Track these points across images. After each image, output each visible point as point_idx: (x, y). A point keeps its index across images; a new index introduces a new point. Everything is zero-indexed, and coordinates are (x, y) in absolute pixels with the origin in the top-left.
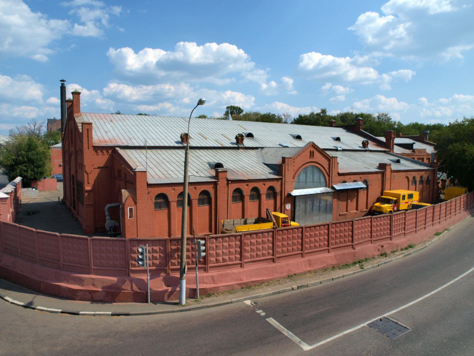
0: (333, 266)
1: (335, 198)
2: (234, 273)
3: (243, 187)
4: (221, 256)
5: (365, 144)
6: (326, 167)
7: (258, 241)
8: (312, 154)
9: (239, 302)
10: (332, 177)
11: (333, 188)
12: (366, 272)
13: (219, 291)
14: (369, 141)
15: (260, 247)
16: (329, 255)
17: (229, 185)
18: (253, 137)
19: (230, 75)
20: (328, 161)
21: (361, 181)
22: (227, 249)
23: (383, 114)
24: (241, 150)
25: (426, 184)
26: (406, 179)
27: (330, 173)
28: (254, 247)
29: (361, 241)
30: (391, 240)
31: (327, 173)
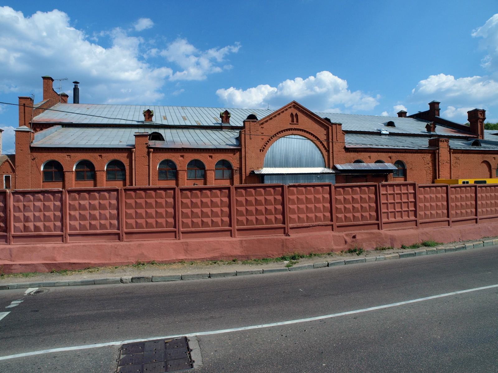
0: (234, 259)
2: (45, 248)
3: (176, 158)
4: (31, 221)
6: (323, 137)
7: (92, 203)
8: (294, 118)
9: (20, 288)
10: (333, 152)
11: (334, 168)
13: (13, 271)
15: (96, 213)
16: (228, 239)
17: (151, 154)
20: (325, 130)
21: (392, 163)
22: (40, 211)
26: (485, 166)
27: (329, 148)
28: (86, 213)
30: (379, 229)
31: (324, 147)
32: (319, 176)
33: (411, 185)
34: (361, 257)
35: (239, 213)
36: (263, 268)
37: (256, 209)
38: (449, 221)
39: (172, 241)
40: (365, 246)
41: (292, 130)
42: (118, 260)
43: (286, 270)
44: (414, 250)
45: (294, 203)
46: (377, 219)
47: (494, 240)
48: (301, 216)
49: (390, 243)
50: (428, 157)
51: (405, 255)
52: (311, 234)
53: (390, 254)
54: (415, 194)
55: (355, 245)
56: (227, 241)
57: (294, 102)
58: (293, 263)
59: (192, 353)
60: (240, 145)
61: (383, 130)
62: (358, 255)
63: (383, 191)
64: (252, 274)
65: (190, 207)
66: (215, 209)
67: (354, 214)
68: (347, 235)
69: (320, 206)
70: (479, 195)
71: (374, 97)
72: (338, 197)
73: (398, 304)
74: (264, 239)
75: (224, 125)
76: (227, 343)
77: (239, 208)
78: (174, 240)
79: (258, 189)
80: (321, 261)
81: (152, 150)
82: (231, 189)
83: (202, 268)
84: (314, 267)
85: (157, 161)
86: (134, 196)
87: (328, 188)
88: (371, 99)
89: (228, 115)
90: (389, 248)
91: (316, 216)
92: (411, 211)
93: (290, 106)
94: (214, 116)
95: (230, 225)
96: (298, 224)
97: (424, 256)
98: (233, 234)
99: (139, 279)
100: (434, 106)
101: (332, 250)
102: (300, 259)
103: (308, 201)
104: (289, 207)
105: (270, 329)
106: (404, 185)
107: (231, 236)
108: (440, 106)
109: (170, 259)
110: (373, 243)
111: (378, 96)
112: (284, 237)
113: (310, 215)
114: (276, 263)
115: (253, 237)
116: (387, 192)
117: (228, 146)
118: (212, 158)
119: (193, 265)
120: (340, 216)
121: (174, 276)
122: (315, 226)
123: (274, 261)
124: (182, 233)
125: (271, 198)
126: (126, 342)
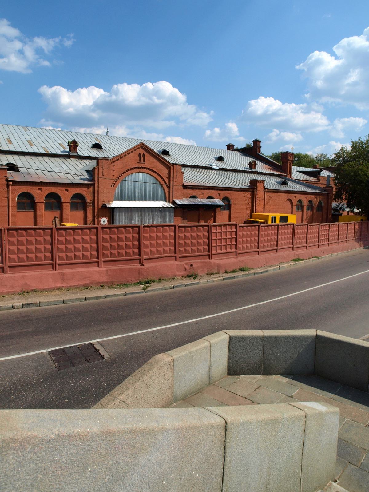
0: (102, 285)
1: (179, 216)
3: (34, 191)
5: (252, 165)
6: (165, 176)
8: (142, 158)
10: (173, 189)
11: (174, 203)
12: (148, 293)
14: (257, 161)
16: (97, 269)
17: (10, 187)
18: (102, 148)
19: (170, 118)
20: (167, 169)
23: (322, 155)
24: (74, 160)
25: (318, 211)
26: (289, 202)
29: (155, 256)
30: (209, 259)
31: (166, 183)
32: (160, 210)
33: (234, 225)
34: (196, 281)
35: (105, 248)
36: (125, 291)
37: (118, 245)
38: (258, 251)
39: (51, 272)
40: (199, 272)
41: (139, 169)
42: (5, 290)
43: (143, 292)
44: (233, 274)
45: (147, 240)
46: (209, 252)
47: (286, 265)
48: (152, 249)
49: (217, 269)
50: (248, 194)
51: (227, 278)
52: (160, 263)
53: (217, 277)
54: (236, 232)
55: (192, 272)
56: (96, 271)
57: (142, 144)
58: (147, 287)
59: (100, 351)
60: (93, 180)
61: (214, 165)
62: (194, 279)
63: (214, 230)
64: (118, 296)
65: (65, 243)
66: (85, 245)
67: (192, 248)
68: (186, 264)
69: (167, 241)
70: (280, 232)
71: (208, 113)
72: (180, 235)
73: (222, 313)
74: (124, 269)
75: (72, 154)
76: (121, 344)
77: (105, 244)
78: (51, 271)
79: (120, 229)
80: (168, 284)
81: (11, 183)
82: (99, 229)
83: (77, 293)
84: (163, 289)
85: (15, 193)
86: (16, 235)
87: (173, 227)
88: (205, 115)
89: (76, 145)
90: (216, 273)
91: (164, 249)
92: (233, 238)
93: (138, 147)
94: (60, 142)
95: (98, 258)
96: (150, 256)
97: (240, 279)
98: (100, 265)
99: (28, 305)
100: (257, 143)
101: (176, 276)
102: (152, 283)
103: (158, 238)
104: (144, 243)
105: (145, 333)
106: (229, 225)
107: (98, 266)
108: (262, 144)
109: (50, 287)
110: (205, 269)
111: (212, 112)
113: (159, 249)
114: (134, 287)
115: (116, 267)
116: (216, 230)
117: (82, 180)
118: (68, 192)
119: (70, 291)
120: (181, 249)
121: (57, 301)
122: (163, 257)
123: (132, 285)
124: (58, 265)
125: (130, 236)
126: (50, 350)
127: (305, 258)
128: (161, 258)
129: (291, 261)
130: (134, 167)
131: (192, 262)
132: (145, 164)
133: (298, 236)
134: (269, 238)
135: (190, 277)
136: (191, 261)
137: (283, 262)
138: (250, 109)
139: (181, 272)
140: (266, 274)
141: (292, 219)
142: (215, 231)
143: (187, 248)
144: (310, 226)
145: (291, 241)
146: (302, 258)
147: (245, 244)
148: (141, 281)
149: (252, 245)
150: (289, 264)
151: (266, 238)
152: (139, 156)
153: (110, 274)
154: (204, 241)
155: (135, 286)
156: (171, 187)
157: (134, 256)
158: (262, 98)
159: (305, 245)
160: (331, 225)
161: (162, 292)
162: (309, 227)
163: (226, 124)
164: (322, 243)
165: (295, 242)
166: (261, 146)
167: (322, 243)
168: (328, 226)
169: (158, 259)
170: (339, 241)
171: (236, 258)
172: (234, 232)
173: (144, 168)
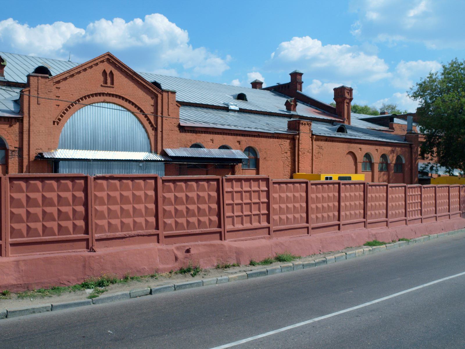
6: (149, 109)
10: (162, 132)
11: (164, 154)
12: (97, 306)
20: (152, 98)
21: (241, 150)
23: (389, 106)
25: (396, 171)
26: (350, 157)
27: (157, 124)
29: (119, 234)
30: (221, 239)
31: (150, 123)
33: (263, 179)
34: (197, 279)
40: (202, 264)
43: (88, 303)
44: (265, 266)
45: (102, 203)
47: (357, 251)
51: (255, 273)
53: (236, 273)
55: (189, 263)
58: (99, 292)
60: (21, 112)
61: (232, 105)
62: (193, 276)
63: (228, 187)
64: (34, 312)
67: (189, 219)
68: (178, 249)
69: (141, 207)
70: (342, 195)
71: (223, 58)
72: (167, 195)
73: (244, 341)
74: (55, 258)
84: (130, 296)
87: (153, 181)
88: (219, 61)
89: (2, 63)
90: (234, 266)
91: (135, 222)
92: (263, 214)
93: (102, 59)
97: (278, 275)
100: (296, 76)
101: (157, 271)
103: (124, 200)
104: (96, 209)
108: (304, 79)
111: (229, 57)
112: (86, 253)
114: (73, 293)
120: (169, 221)
122: (133, 236)
125: (67, 195)
127: (386, 241)
128: (130, 237)
129: (364, 245)
130: (94, 93)
131: (187, 246)
132: (114, 89)
133: (373, 204)
134: (325, 205)
135: (185, 272)
136: (187, 243)
137: (351, 247)
138: (282, 53)
139: (168, 264)
140: (323, 266)
141: (359, 177)
142: (230, 189)
143: (179, 220)
144: (390, 187)
145: (362, 211)
146: (381, 241)
147: (284, 214)
148: (88, 280)
149: (297, 216)
150: (362, 250)
151: (320, 205)
152: (103, 75)
153: (23, 268)
154: (210, 208)
155: (74, 291)
156: (159, 129)
157: (76, 234)
158: (297, 39)
159: (385, 219)
160: (424, 188)
161: (128, 301)
162: (389, 189)
163: (248, 74)
164: (411, 217)
165: (369, 213)
166: (303, 80)
167: (411, 218)
168: (419, 189)
169: (124, 240)
170: (438, 215)
171: (270, 238)
172: (265, 193)
173: (113, 95)
